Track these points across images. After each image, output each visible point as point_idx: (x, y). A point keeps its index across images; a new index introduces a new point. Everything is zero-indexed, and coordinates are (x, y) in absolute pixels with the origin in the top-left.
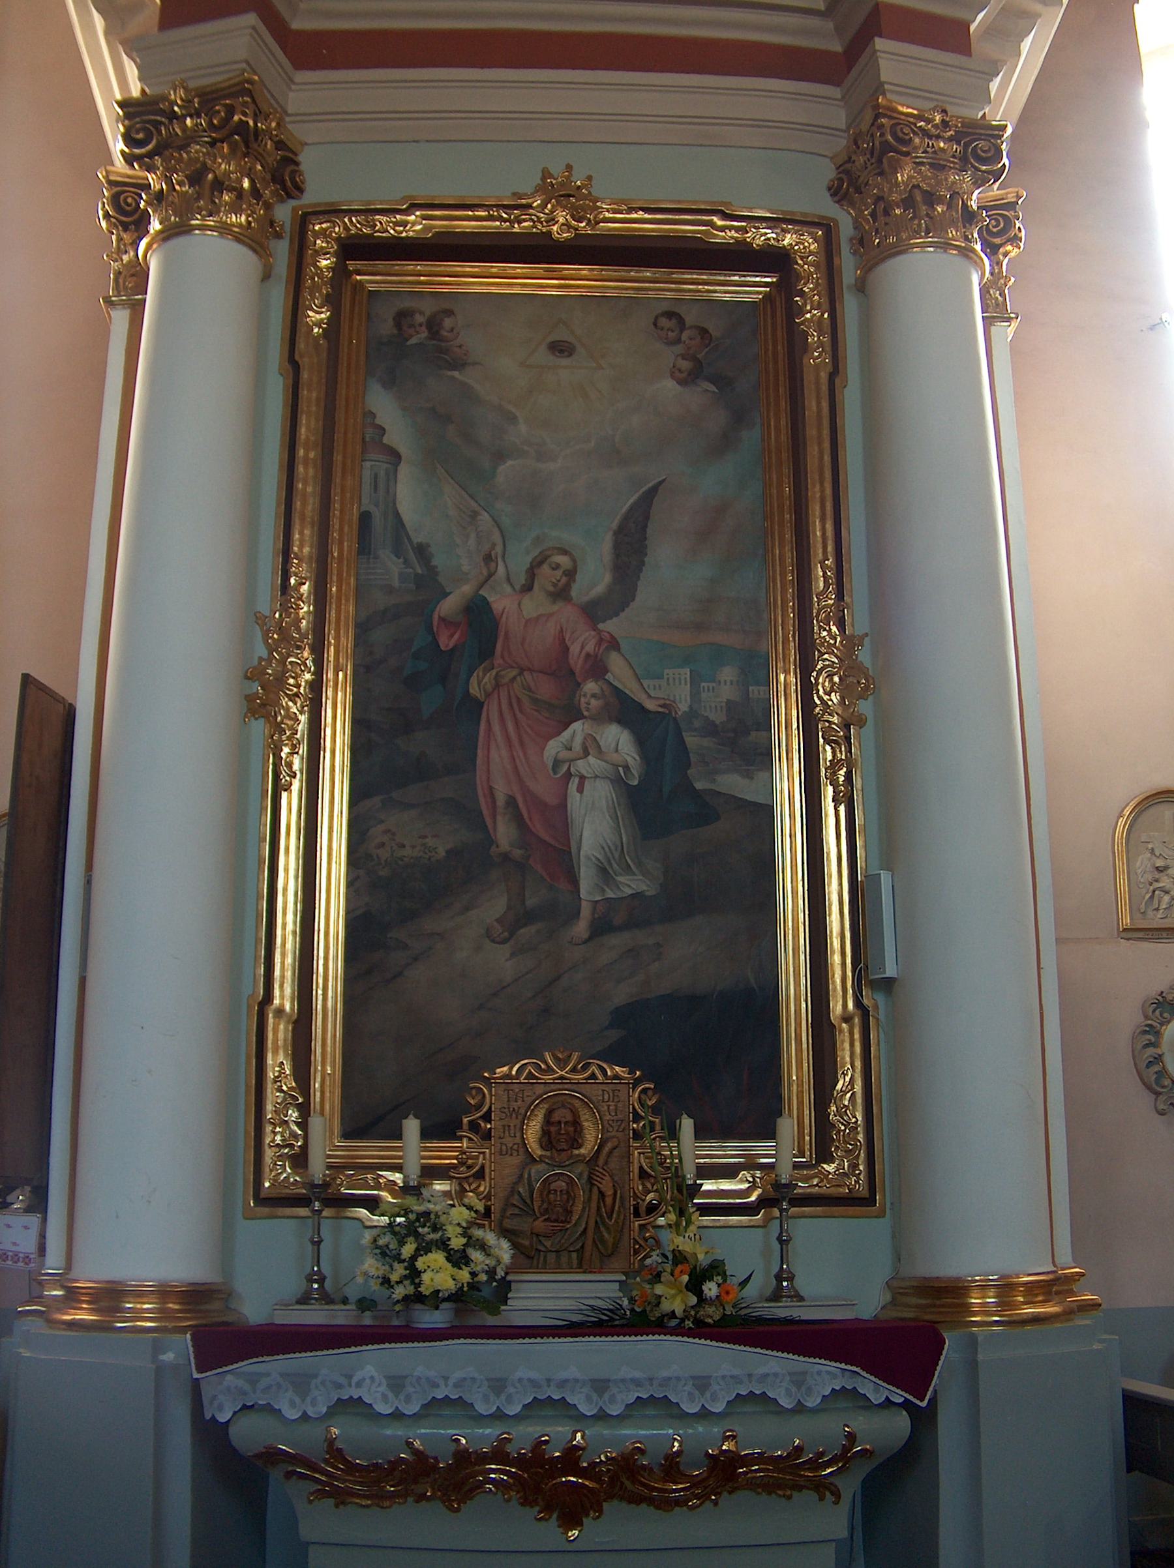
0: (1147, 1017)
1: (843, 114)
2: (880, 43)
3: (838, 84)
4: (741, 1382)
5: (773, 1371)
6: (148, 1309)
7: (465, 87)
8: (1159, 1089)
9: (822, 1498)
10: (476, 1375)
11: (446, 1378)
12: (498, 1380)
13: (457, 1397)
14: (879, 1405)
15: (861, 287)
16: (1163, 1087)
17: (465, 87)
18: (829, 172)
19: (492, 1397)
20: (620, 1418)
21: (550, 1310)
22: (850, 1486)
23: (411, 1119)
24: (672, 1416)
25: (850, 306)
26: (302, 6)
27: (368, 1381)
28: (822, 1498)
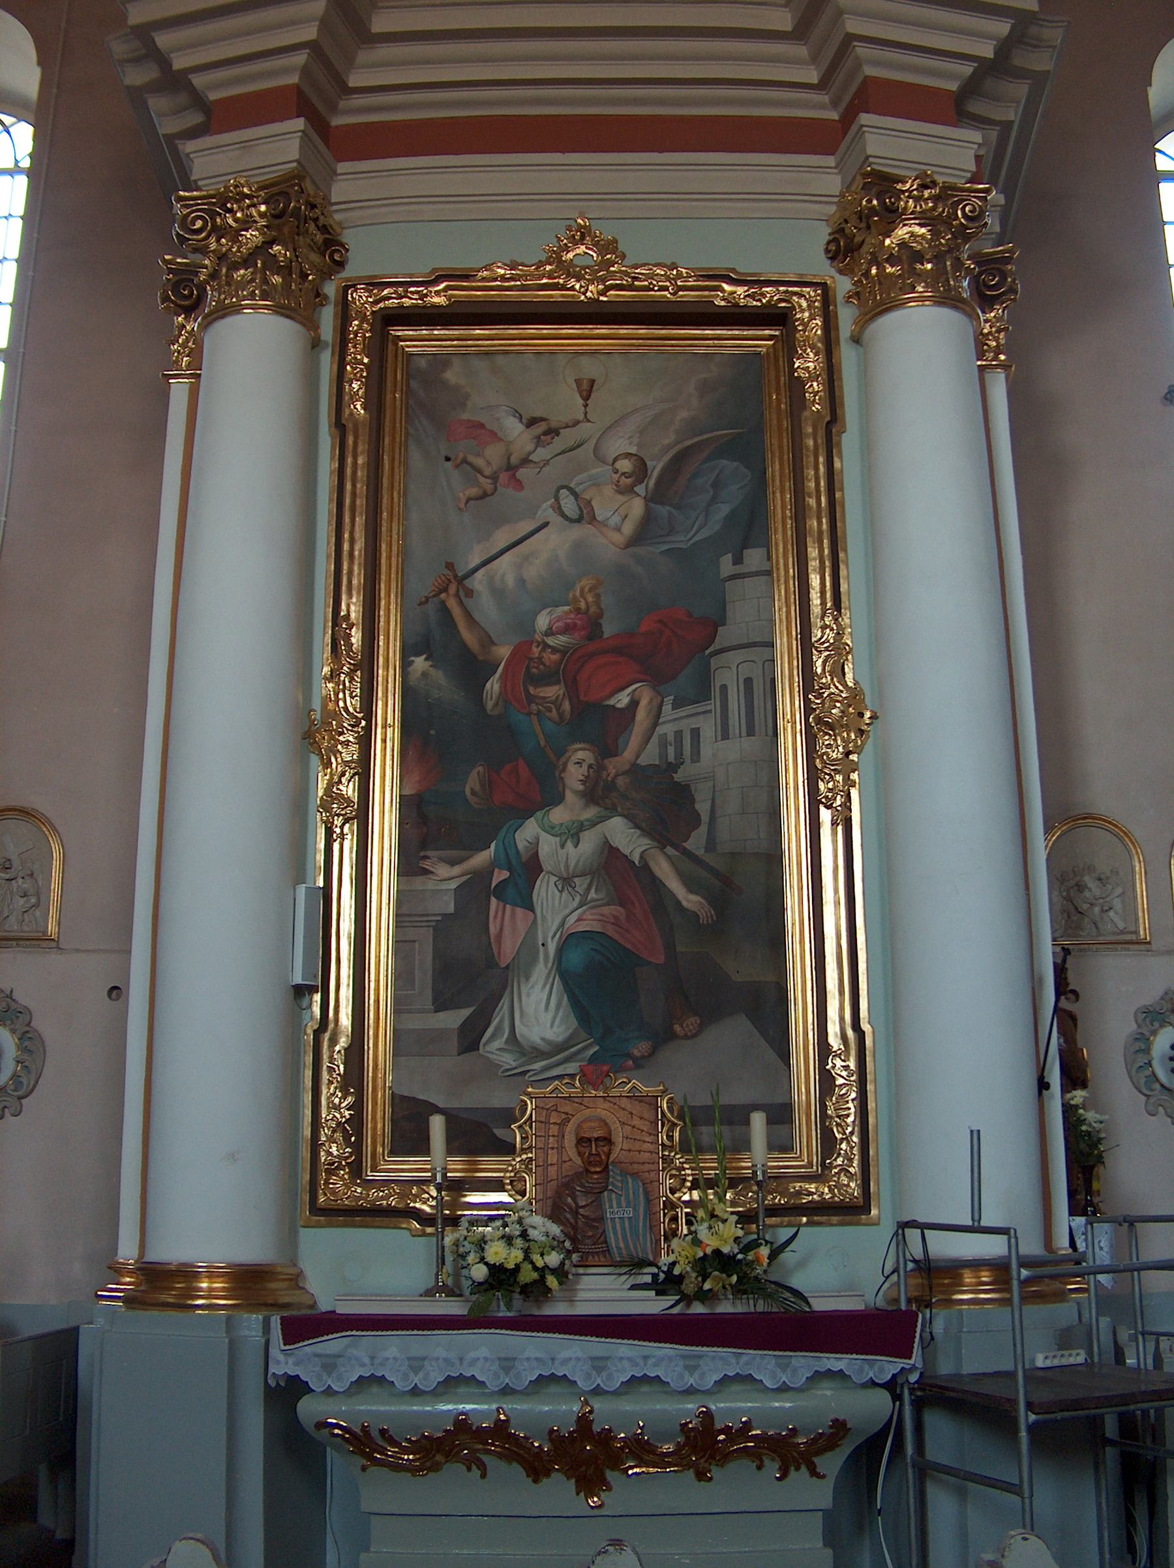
0: (1139, 1026)
1: (838, 180)
2: (865, 118)
3: (831, 153)
4: (637, 1365)
5: (483, 1355)
6: (217, 1288)
7: (357, 179)
8: (1149, 1093)
9: (469, 1469)
10: (398, 1355)
11: (461, 1359)
12: (506, 1359)
13: (734, 1373)
14: (404, 1393)
15: (856, 340)
16: (1152, 1090)
17: (357, 179)
18: (824, 233)
19: (412, 1375)
20: (616, 1393)
21: (609, 1290)
22: (832, 1463)
23: (1154, 1039)
24: (666, 1393)
25: (847, 355)
26: (380, 23)
27: (482, 1361)
28: (469, 1469)
